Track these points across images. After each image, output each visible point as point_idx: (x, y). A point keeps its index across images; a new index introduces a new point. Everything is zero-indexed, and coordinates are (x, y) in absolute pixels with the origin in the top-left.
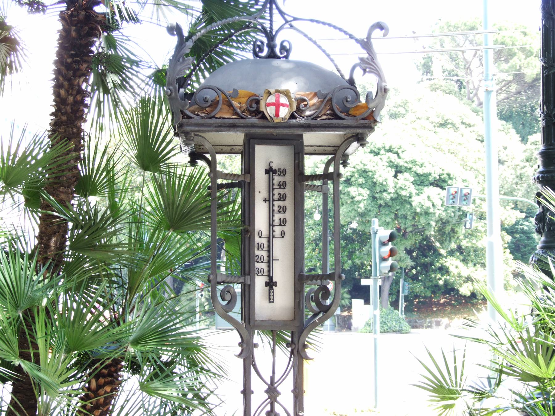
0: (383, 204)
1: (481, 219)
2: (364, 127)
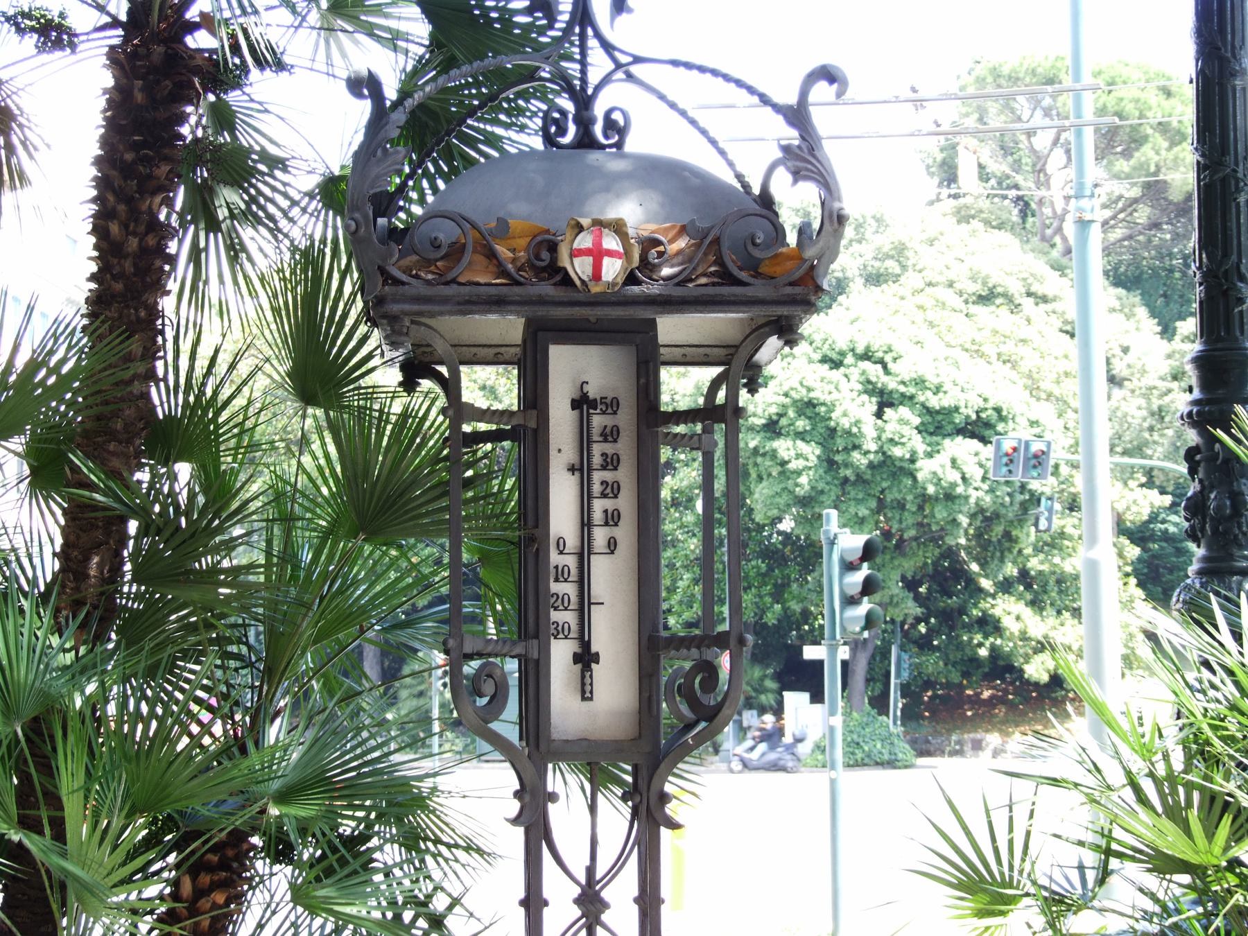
0: (853, 478)
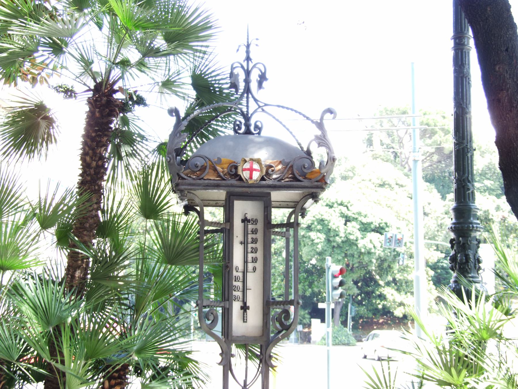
0: (336, 246)
1: (411, 258)
2: (317, 187)
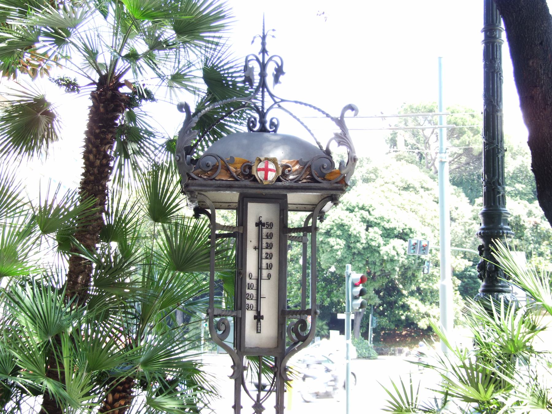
0: (357, 253)
1: (436, 266)
2: (337, 189)
